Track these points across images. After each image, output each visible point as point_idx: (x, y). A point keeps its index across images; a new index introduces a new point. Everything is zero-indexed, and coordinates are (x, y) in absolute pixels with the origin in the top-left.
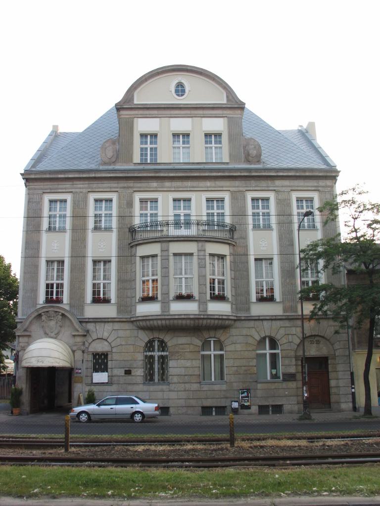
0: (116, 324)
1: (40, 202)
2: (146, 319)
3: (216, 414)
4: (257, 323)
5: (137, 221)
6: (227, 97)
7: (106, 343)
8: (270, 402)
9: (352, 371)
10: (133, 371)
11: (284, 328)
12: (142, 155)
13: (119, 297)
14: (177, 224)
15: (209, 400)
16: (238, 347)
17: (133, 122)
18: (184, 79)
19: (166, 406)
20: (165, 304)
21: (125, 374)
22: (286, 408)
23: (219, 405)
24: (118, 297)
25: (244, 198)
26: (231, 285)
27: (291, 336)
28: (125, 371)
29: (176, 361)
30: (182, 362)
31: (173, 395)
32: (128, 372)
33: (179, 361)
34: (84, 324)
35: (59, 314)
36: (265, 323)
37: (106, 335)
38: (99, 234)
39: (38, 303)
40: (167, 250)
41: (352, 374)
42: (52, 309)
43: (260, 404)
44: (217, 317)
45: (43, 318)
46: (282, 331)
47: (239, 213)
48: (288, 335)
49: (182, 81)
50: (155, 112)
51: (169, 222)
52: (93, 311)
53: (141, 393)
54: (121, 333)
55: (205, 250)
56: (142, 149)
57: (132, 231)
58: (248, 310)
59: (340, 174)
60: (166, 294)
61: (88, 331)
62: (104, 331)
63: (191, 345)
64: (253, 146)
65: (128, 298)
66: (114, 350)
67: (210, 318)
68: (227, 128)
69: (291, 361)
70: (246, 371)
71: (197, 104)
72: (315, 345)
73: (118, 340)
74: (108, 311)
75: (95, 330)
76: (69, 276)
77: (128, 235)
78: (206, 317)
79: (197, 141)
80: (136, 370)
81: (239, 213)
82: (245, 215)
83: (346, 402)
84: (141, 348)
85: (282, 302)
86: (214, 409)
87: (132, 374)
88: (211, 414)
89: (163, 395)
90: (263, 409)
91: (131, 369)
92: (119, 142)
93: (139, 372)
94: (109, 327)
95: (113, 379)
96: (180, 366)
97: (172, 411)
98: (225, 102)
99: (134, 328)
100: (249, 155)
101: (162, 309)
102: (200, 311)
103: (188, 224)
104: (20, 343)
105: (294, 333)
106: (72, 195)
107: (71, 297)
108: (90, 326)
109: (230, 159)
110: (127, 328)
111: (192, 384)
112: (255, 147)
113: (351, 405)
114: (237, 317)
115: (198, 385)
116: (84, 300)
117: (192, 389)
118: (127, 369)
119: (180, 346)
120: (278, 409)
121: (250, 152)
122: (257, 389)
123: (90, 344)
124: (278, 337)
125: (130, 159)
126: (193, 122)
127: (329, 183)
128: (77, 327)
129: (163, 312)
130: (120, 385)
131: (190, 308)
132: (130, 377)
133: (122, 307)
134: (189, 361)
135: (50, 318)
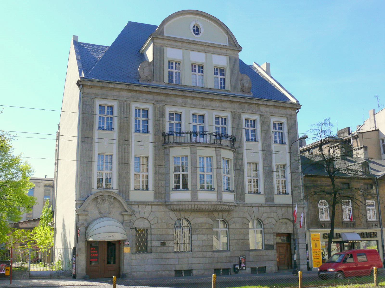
0: (154, 207)
1: (92, 105)
2: (180, 203)
3: (223, 275)
4: (250, 209)
5: (167, 130)
6: (229, 41)
7: (147, 221)
8: (258, 265)
9: (307, 243)
10: (166, 243)
11: (266, 213)
12: (169, 76)
13: (155, 186)
14: (195, 134)
15: (220, 264)
16: (238, 226)
17: (163, 50)
18: (201, 22)
19: (190, 269)
20: (219, 193)
21: (161, 245)
22: (268, 269)
23: (226, 267)
24: (154, 186)
25: (241, 118)
26: (234, 182)
27: (270, 218)
28: (161, 243)
29: (197, 235)
30: (200, 236)
31: (195, 261)
32: (163, 244)
33: (199, 235)
34: (130, 206)
35: (111, 198)
36: (254, 208)
37: (146, 215)
38: (137, 134)
39: (92, 188)
40: (195, 153)
41: (307, 245)
42: (106, 194)
43: (252, 266)
44: (228, 204)
45: (99, 200)
46: (265, 215)
47: (237, 127)
48: (269, 218)
49: (199, 23)
50: (180, 44)
51: (197, 132)
52: (134, 196)
53: (172, 259)
54: (158, 214)
55: (220, 155)
56: (169, 72)
57: (164, 135)
58: (243, 199)
59: (301, 107)
60: (194, 186)
61: (134, 211)
62: (145, 211)
63: (207, 224)
64: (246, 81)
65: (162, 187)
66: (153, 227)
67: (225, 204)
68: (229, 64)
69: (271, 236)
70: (242, 243)
71: (210, 44)
72: (284, 225)
73: (156, 219)
74: (149, 196)
75: (138, 211)
76: (117, 168)
77: (162, 138)
78: (222, 203)
79: (209, 72)
80: (168, 242)
81: (237, 127)
82: (241, 128)
83: (303, 265)
84: (172, 225)
85: (191, 190)
86: (183, 272)
87: (166, 245)
88: (256, 273)
89: (188, 260)
90: (253, 270)
91: (165, 241)
92: (153, 65)
93: (171, 243)
94: (148, 208)
95: (152, 249)
96: (200, 239)
97: (194, 272)
98: (227, 45)
99: (167, 210)
100: (243, 86)
101: (192, 197)
102: (218, 199)
103: (203, 134)
104: (80, 220)
105: (272, 216)
106: (118, 102)
107: (119, 185)
108: (135, 208)
109: (231, 88)
110: (162, 210)
111: (207, 252)
112: (247, 82)
113: (306, 266)
114: (237, 204)
115: (212, 253)
116: (129, 188)
117: (208, 256)
118: (162, 241)
119: (199, 224)
120: (263, 270)
121: (244, 85)
122: (250, 256)
123: (134, 222)
124: (263, 219)
125: (162, 79)
126: (206, 56)
127: (293, 112)
128: (126, 208)
129: (192, 199)
130: (157, 254)
131: (211, 196)
132: (164, 248)
133: (157, 194)
134: (206, 236)
135: (104, 200)
